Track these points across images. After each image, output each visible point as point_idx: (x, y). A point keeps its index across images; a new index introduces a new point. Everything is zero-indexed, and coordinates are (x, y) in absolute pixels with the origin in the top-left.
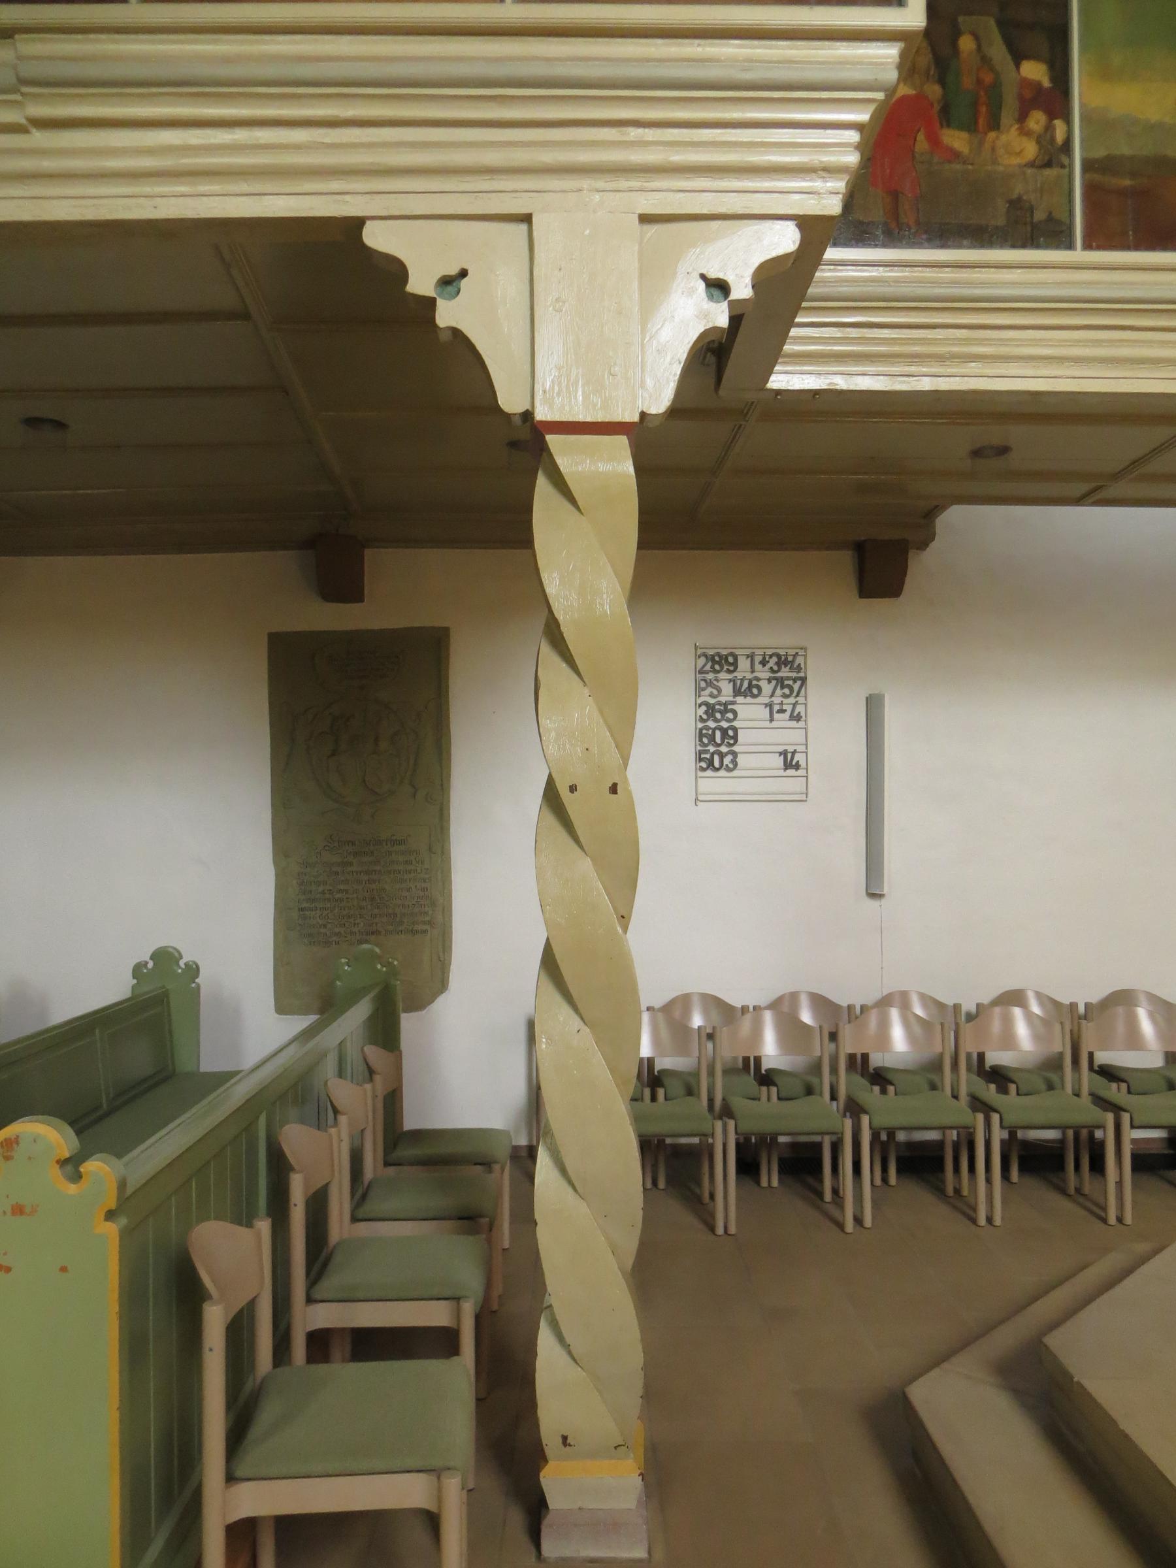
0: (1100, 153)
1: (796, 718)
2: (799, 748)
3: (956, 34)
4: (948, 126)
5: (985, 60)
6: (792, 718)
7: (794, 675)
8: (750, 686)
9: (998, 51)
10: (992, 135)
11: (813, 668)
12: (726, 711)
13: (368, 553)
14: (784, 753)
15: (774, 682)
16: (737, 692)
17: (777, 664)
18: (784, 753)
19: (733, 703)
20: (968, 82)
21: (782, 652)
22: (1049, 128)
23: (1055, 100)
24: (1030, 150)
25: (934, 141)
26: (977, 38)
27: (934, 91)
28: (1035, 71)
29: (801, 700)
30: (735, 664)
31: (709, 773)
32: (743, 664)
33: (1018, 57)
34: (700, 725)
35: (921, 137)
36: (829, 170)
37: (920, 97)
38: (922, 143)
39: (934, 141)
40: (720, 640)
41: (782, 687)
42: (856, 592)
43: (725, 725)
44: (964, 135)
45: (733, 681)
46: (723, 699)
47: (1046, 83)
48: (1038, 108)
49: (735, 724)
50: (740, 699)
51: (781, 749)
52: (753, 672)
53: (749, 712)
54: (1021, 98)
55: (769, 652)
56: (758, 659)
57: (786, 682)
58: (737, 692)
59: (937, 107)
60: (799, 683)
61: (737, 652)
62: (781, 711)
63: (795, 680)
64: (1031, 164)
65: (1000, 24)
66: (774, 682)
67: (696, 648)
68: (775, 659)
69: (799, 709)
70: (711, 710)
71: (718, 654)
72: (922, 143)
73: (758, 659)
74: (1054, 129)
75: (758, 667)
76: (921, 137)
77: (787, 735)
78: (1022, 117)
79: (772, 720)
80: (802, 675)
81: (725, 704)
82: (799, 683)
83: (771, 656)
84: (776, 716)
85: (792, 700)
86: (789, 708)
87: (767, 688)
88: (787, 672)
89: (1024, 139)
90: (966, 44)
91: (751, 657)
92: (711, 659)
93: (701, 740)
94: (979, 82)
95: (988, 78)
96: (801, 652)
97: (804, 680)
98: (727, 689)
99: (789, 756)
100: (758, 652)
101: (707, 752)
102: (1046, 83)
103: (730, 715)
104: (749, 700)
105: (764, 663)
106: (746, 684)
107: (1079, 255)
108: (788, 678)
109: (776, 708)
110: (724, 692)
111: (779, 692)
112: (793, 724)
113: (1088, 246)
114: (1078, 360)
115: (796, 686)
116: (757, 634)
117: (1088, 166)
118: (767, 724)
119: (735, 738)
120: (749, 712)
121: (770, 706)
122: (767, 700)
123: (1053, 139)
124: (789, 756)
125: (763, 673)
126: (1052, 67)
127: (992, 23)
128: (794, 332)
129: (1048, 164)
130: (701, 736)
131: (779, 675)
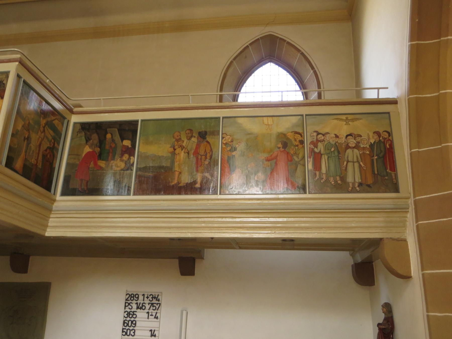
0: (143, 165)
1: (156, 318)
2: (156, 329)
3: (106, 133)
4: (100, 159)
5: (113, 140)
6: (155, 317)
7: (157, 302)
8: (143, 306)
9: (117, 138)
10: (112, 162)
11: (164, 300)
12: (134, 314)
13: (31, 258)
14: (151, 331)
15: (150, 305)
16: (138, 308)
17: (152, 298)
18: (151, 331)
19: (136, 312)
20: (107, 147)
21: (153, 294)
22: (129, 159)
23: (130, 151)
24: (123, 165)
25: (96, 164)
26: (112, 135)
27: (98, 150)
28: (127, 143)
29: (159, 311)
30: (138, 298)
31: (126, 336)
32: (141, 298)
33: (122, 139)
34: (125, 319)
35: (92, 163)
36: (268, 120)
37: (94, 152)
38: (92, 165)
39: (96, 164)
40: (133, 290)
41: (153, 306)
42: (180, 274)
43: (132, 319)
44: (104, 162)
45: (137, 303)
46: (132, 310)
47: (130, 146)
48: (127, 154)
49: (136, 319)
50: (139, 310)
51: (150, 329)
52: (144, 300)
53: (141, 315)
54: (122, 151)
55: (149, 294)
56: (146, 296)
57: (154, 305)
58: (138, 308)
59: (98, 154)
60: (158, 305)
61: (138, 293)
62: (152, 315)
63: (157, 304)
64: (122, 170)
65: (119, 130)
66: (150, 305)
67: (127, 291)
68: (151, 296)
69: (158, 315)
70: (129, 314)
71: (132, 294)
72: (92, 165)
73: (146, 296)
74: (130, 159)
75: (146, 299)
76: (92, 163)
77: (152, 324)
78: (122, 155)
79: (148, 318)
80: (160, 302)
81: (134, 312)
82: (158, 305)
83: (150, 295)
84: (150, 317)
85: (156, 311)
86: (154, 314)
87: (148, 306)
88: (155, 301)
89: (121, 163)
90: (109, 136)
91: (144, 295)
92: (130, 295)
93: (124, 325)
94: (111, 147)
95: (113, 145)
96: (160, 294)
97: (160, 304)
98: (134, 306)
99: (153, 332)
100: (145, 294)
101: (125, 329)
102: (130, 146)
103: (135, 316)
104: (142, 310)
105: (148, 298)
106: (141, 305)
107: (132, 197)
108: (155, 303)
109: (150, 314)
110: (133, 307)
111: (152, 308)
112: (156, 320)
113: (134, 194)
114: (137, 227)
115: (157, 307)
116: (145, 287)
117: (138, 169)
118: (147, 320)
119: (135, 324)
120: (141, 315)
121: (148, 313)
122: (147, 311)
123: (130, 162)
124: (153, 332)
125: (147, 301)
126: (132, 142)
127: (116, 129)
128: (51, 219)
129: (127, 170)
130: (124, 323)
131: (152, 302)
